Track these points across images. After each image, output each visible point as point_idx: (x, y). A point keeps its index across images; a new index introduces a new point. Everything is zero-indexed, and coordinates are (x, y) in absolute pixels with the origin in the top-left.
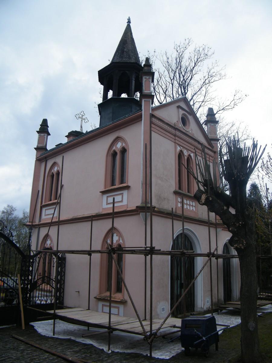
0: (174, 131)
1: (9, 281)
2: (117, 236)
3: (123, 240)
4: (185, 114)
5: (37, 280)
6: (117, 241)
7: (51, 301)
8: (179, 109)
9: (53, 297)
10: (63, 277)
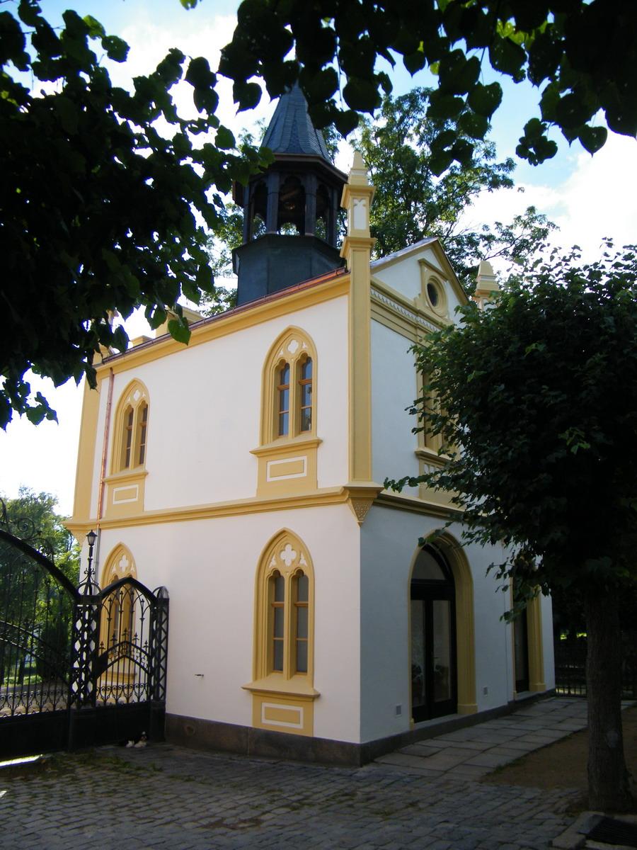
0: (414, 317)
1: (138, 655)
2: (292, 550)
3: (309, 558)
4: (436, 278)
5: (108, 650)
6: (293, 562)
7: (139, 698)
8: (423, 266)
9: (142, 689)
10: (164, 642)
